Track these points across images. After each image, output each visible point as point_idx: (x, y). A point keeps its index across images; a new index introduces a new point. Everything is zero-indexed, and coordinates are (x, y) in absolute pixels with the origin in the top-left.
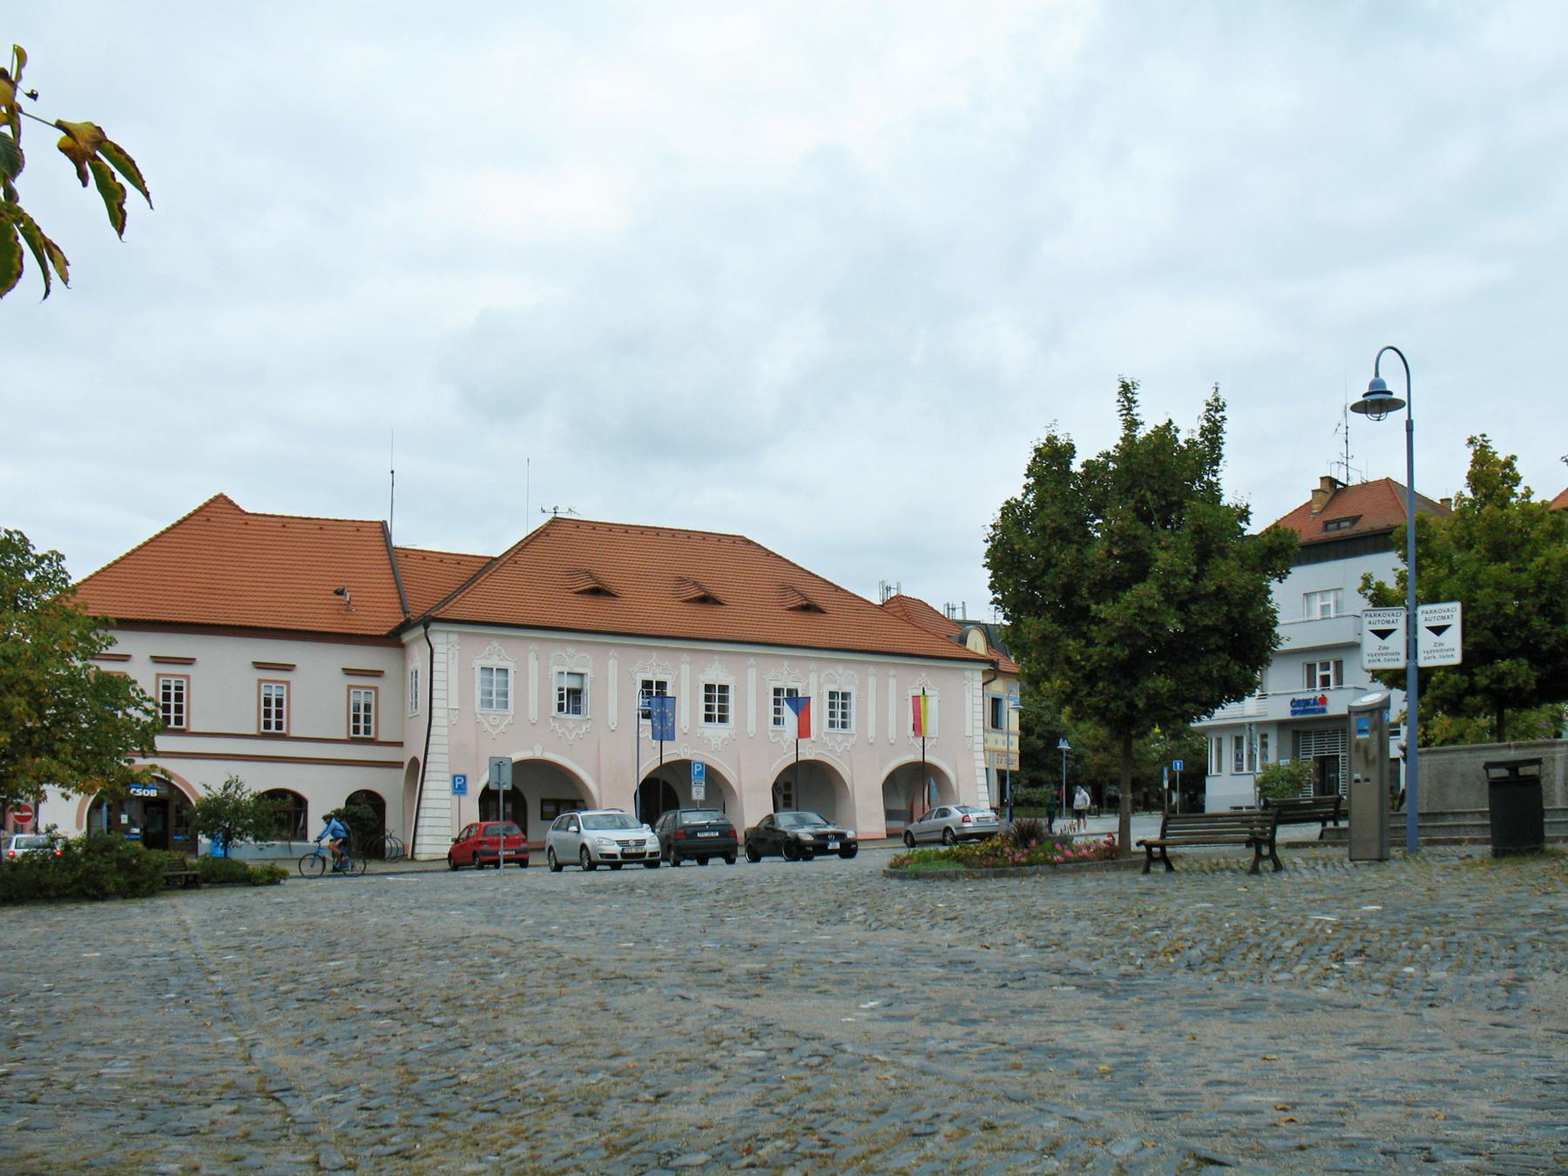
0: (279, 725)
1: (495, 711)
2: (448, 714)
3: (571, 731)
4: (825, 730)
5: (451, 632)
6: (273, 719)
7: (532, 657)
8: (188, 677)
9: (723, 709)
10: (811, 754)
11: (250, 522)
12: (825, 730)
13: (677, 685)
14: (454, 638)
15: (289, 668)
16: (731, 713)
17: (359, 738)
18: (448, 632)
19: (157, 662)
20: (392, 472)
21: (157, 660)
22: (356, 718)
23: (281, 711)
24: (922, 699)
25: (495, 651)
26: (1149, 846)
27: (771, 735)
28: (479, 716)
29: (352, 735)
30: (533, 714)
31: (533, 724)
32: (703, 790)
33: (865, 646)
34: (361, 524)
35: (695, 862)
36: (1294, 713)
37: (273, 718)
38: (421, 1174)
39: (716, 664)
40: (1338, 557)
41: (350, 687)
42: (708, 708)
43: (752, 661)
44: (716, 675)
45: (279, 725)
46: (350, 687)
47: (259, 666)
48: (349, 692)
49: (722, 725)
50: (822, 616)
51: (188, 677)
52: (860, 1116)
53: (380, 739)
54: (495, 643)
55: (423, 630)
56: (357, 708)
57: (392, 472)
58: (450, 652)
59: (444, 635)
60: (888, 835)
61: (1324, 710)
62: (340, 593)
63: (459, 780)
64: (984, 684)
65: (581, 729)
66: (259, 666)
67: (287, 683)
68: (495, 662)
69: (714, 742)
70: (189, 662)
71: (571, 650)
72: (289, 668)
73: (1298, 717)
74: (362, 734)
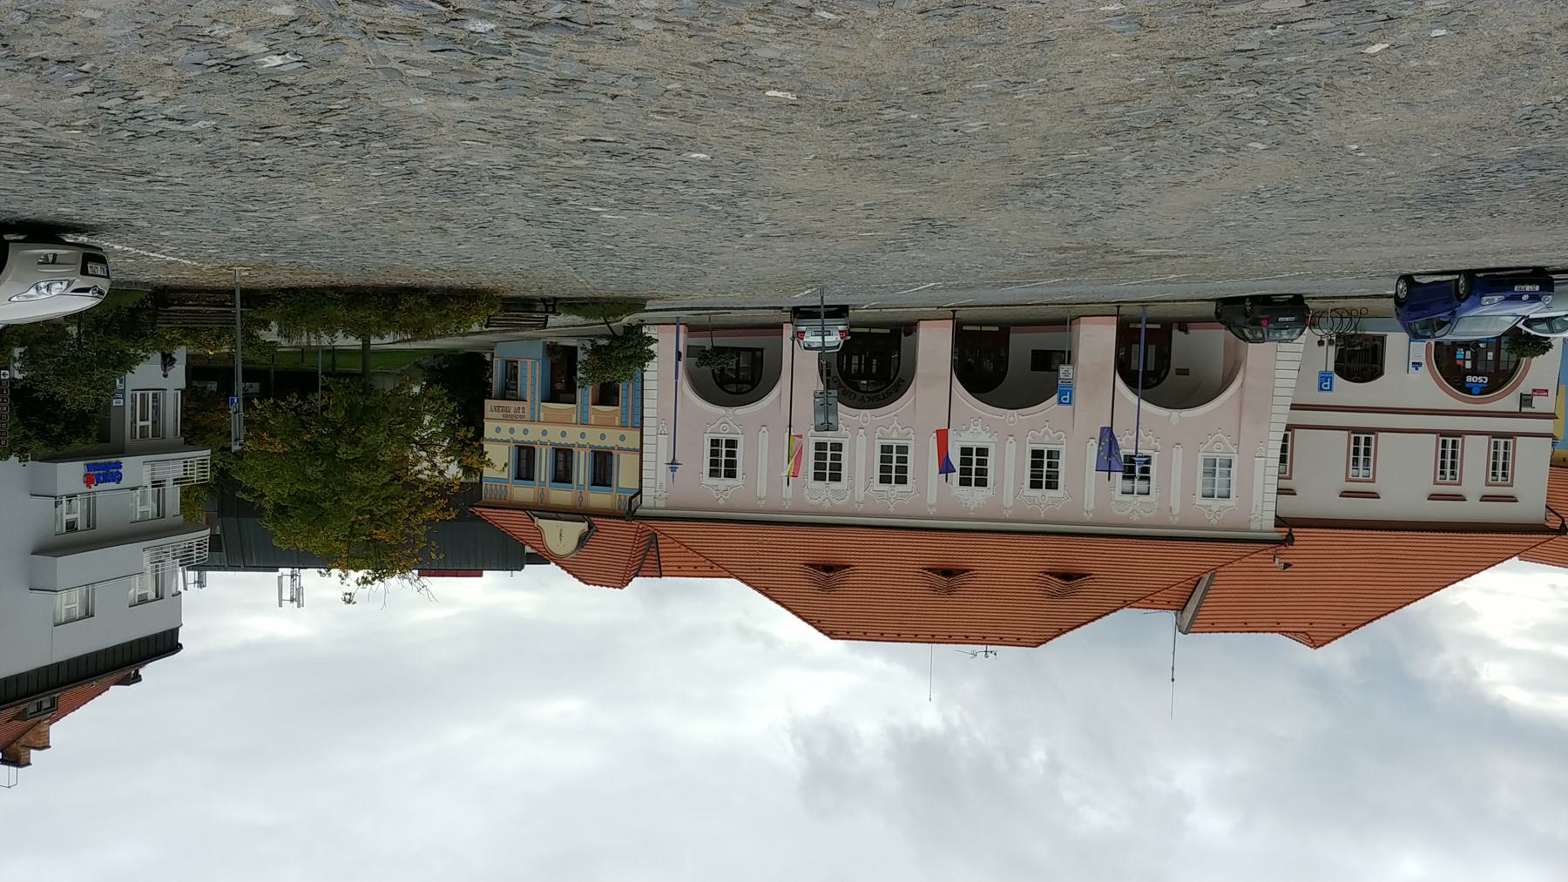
0: (1357, 441)
1: (1219, 455)
2: (1266, 452)
3: (1046, 433)
4: (912, 442)
5: (1258, 532)
6: (1449, 450)
7: (1176, 510)
8: (1487, 484)
9: (714, 453)
10: (865, 415)
11: (1210, 625)
12: (912, 442)
13: (869, 478)
14: (1255, 526)
15: (1346, 494)
16: (708, 448)
17: (1364, 433)
18: (1261, 531)
19: (1460, 496)
20: (1173, 680)
21: (1460, 498)
22: (1367, 452)
23: (1354, 454)
24: (791, 474)
25: (1216, 514)
26: (554, 312)
27: (912, 435)
28: (1235, 451)
29: (1373, 437)
30: (1178, 454)
31: (1179, 444)
32: (1062, 376)
33: (947, 536)
34: (1243, 629)
35: (1311, 305)
36: (119, 465)
37: (1362, 445)
38: (766, 9)
39: (972, 508)
40: (96, 655)
41: (1373, 481)
42: (733, 454)
43: (932, 512)
44: (973, 499)
45: (1357, 441)
46: (1373, 481)
47: (1373, 495)
48: (1512, 481)
49: (967, 445)
50: (927, 564)
51: (1487, 484)
52: (947, 11)
53: (1346, 433)
54: (1214, 522)
55: (638, 510)
56: (1367, 461)
57: (1173, 680)
58: (1260, 512)
59: (1264, 528)
60: (782, 327)
61: (88, 465)
62: (1287, 565)
63: (1326, 386)
64: (640, 492)
65: (1127, 439)
66: (1373, 495)
67: (1348, 480)
68: (1215, 504)
69: (979, 427)
70: (1433, 497)
71: (1135, 518)
72: (1346, 494)
73: (114, 460)
74: (1363, 437)
